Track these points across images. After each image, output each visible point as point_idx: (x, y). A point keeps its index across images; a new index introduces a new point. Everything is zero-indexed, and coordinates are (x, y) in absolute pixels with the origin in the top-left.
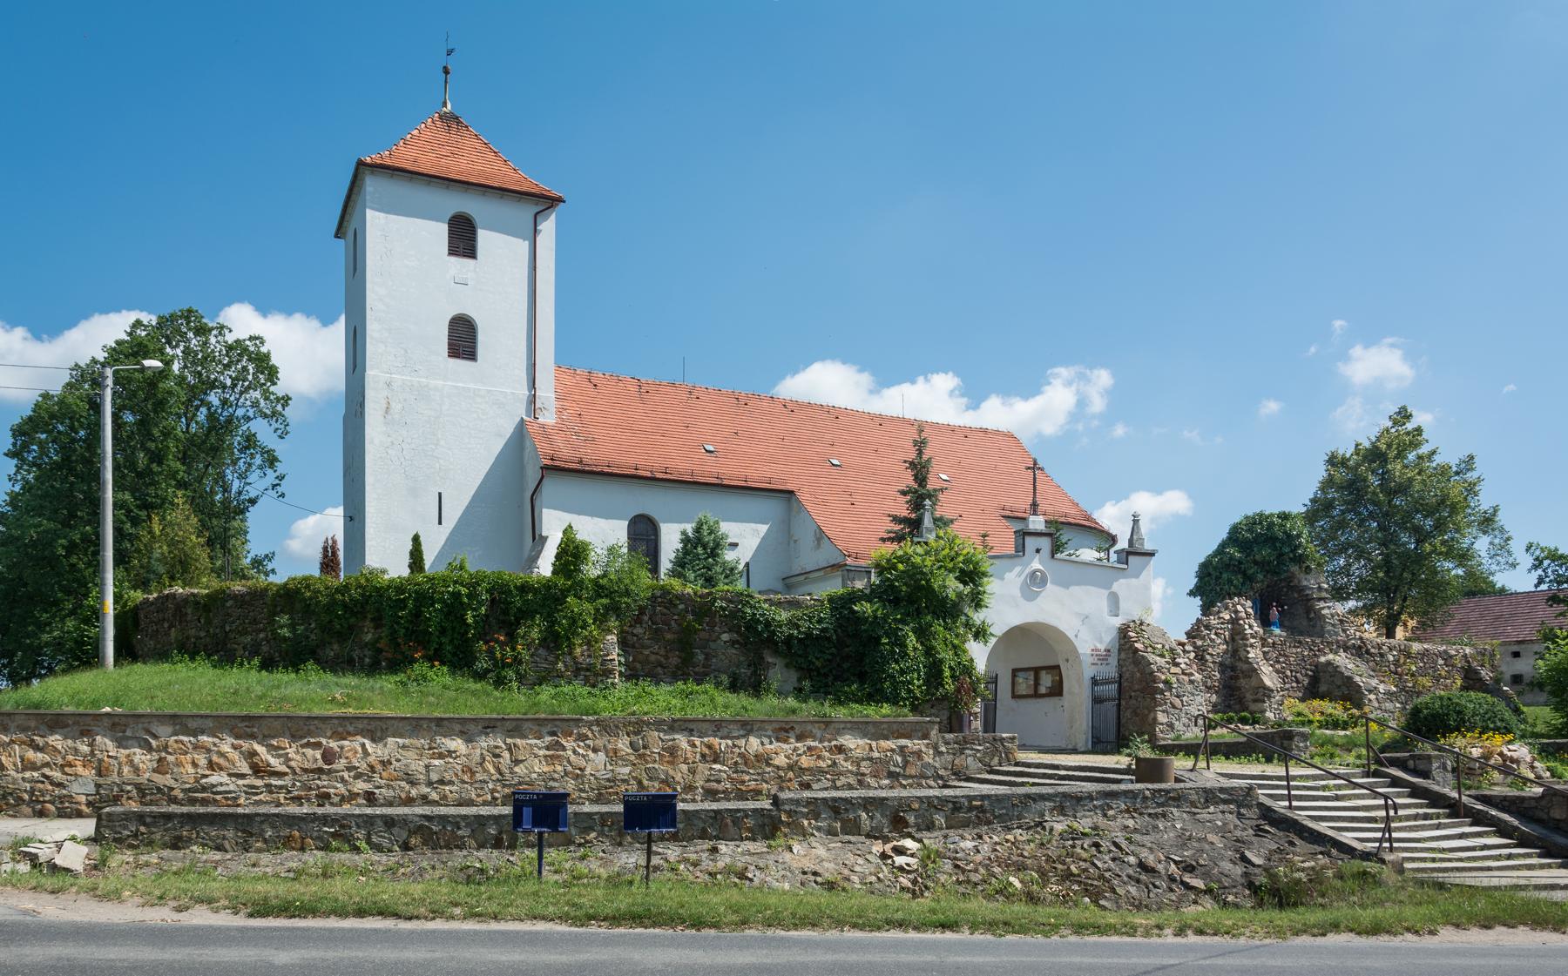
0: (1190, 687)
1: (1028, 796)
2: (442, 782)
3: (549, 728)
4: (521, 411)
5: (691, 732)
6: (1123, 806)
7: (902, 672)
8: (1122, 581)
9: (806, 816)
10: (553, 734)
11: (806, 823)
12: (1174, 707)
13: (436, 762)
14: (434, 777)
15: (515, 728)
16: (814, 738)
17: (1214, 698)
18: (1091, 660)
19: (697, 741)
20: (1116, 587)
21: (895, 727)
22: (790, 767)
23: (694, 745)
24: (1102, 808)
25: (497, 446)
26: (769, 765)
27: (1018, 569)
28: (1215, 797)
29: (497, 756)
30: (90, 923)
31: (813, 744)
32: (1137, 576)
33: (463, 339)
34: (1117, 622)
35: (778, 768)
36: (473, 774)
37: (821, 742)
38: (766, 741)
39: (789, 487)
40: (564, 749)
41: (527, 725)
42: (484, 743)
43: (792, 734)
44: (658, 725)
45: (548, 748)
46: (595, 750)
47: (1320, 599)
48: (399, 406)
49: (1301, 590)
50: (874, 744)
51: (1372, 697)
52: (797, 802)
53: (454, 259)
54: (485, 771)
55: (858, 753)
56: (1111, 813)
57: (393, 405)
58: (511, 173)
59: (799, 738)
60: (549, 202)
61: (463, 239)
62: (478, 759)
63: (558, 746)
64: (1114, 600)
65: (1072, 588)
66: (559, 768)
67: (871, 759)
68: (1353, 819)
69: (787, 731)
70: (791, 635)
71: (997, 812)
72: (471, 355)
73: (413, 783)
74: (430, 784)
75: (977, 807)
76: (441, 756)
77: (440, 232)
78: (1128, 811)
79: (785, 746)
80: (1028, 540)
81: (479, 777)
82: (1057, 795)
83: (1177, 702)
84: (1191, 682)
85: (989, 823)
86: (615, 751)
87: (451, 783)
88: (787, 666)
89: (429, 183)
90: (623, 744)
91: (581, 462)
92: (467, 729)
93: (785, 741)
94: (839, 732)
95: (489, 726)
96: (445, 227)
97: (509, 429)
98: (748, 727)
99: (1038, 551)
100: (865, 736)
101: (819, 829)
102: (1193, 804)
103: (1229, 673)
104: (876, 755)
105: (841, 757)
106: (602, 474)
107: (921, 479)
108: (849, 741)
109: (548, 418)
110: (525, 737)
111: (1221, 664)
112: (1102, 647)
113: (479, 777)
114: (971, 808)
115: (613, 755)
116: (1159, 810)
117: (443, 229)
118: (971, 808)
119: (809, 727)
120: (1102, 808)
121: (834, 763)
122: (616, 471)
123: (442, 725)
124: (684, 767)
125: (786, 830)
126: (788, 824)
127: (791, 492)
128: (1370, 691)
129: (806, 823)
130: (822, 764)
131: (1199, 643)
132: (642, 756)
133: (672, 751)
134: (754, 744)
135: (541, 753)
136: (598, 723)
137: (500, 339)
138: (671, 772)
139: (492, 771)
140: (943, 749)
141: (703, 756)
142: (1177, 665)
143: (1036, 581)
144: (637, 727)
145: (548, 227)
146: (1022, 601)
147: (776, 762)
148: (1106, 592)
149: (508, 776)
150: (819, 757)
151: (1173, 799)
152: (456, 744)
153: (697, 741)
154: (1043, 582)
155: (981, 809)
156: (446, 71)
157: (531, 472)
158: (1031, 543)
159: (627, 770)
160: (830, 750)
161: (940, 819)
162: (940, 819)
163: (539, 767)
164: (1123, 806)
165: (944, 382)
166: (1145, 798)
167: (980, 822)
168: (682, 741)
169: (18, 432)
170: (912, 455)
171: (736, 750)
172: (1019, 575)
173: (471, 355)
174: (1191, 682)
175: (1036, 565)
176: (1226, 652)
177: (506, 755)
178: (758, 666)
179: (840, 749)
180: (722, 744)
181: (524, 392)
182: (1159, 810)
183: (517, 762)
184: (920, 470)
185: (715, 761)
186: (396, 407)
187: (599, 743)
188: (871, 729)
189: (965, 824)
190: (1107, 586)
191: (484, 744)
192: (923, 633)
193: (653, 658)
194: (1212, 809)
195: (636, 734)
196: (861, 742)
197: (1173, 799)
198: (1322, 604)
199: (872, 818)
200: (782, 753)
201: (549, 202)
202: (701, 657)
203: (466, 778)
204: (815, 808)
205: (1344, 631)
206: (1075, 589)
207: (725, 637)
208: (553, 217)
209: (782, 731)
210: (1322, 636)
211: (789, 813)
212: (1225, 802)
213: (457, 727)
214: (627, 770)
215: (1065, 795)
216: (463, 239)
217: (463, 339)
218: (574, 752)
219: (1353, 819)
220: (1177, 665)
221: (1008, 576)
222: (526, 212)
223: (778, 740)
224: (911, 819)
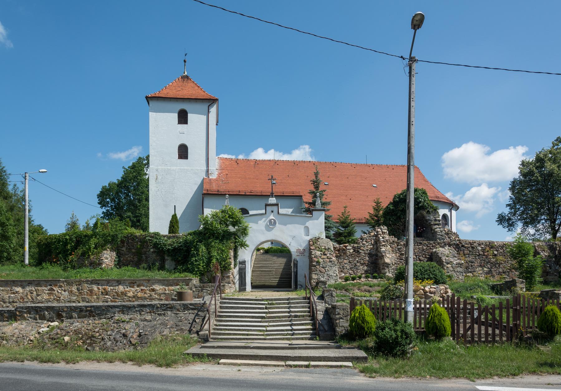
1: (109, 306)
2: (13, 302)
3: (49, 283)
4: (204, 175)
5: (98, 284)
6: (148, 311)
7: (196, 261)
8: (310, 221)
9: (25, 313)
10: (51, 285)
11: (26, 315)
12: (321, 272)
13: (12, 295)
14: (11, 300)
15: (38, 283)
16: (144, 286)
17: (366, 268)
19: (100, 287)
20: (307, 224)
21: (175, 281)
22: (134, 297)
23: (99, 289)
24: (139, 311)
25: (195, 188)
26: (126, 296)
27: (264, 219)
29: (32, 293)
31: (143, 288)
32: (317, 219)
33: (183, 152)
34: (308, 238)
35: (129, 297)
36: (23, 299)
38: (125, 287)
40: (54, 291)
41: (42, 282)
42: (28, 289)
43: (135, 285)
44: (87, 282)
45: (49, 290)
46: (65, 291)
47: (435, 224)
49: (427, 221)
50: (167, 288)
51: (449, 266)
52: (22, 308)
53: (180, 125)
54: (28, 298)
55: (160, 292)
56: (143, 313)
57: (159, 177)
58: (203, 93)
59: (138, 286)
60: (212, 101)
61: (183, 118)
62: (25, 294)
63: (52, 290)
64: (307, 229)
66: (52, 297)
67: (165, 294)
68: (253, 317)
69: (134, 283)
71: (97, 312)
72: (186, 157)
73: (5, 302)
74: (10, 303)
75: (89, 310)
76: (14, 293)
77: (175, 116)
78: (150, 312)
79: (132, 289)
80: (268, 208)
81: (25, 300)
82: (120, 306)
84: (330, 262)
85: (94, 316)
86: (71, 291)
87: (16, 302)
88: (172, 260)
89: (171, 101)
90: (74, 289)
91: (218, 191)
92: (23, 284)
93: (133, 287)
94: (153, 284)
95: (30, 283)
96: (177, 115)
97: (199, 182)
98: (119, 282)
99: (272, 212)
100: (163, 285)
101: (31, 318)
103: (374, 257)
105: (153, 293)
107: (317, 188)
108: (158, 287)
109: (214, 176)
110: (41, 287)
113: (25, 300)
114: (87, 311)
115: (71, 292)
116: (163, 312)
117: (176, 115)
118: (87, 311)
119: (142, 282)
120: (139, 311)
122: (211, 192)
123: (15, 283)
124: (95, 297)
125: (19, 318)
126: (20, 316)
127: (301, 196)
128: (448, 263)
129: (26, 315)
130: (146, 295)
131: (356, 245)
132: (80, 293)
133: (91, 291)
134: (121, 288)
135: (47, 292)
136: (66, 281)
137: (196, 152)
138: (90, 299)
139: (30, 298)
140: (194, 290)
141: (102, 293)
142: (325, 255)
143: (272, 223)
144: (80, 283)
145: (213, 110)
147: (129, 295)
148: (303, 227)
149: (35, 300)
150: (145, 293)
151: (170, 308)
152: (19, 289)
153: (100, 287)
155: (91, 311)
156: (185, 61)
157: (205, 194)
158: (269, 208)
159: (75, 298)
160: (150, 291)
161: (75, 315)
162: (75, 315)
163: (46, 297)
164: (148, 311)
165: (260, 150)
166: (158, 308)
167: (90, 316)
168: (95, 288)
169: (99, 196)
170: (314, 178)
171: (114, 291)
172: (265, 221)
173: (186, 157)
174: (330, 262)
175: (272, 217)
177: (35, 293)
178: (163, 261)
179: (153, 290)
180: (109, 288)
181: (205, 168)
182: (163, 312)
183: (38, 295)
184: (316, 184)
185: (106, 295)
186: (160, 177)
187: (66, 288)
188: (166, 282)
189: (85, 317)
190: (303, 224)
191: (28, 289)
192: (208, 246)
193: (129, 259)
194: (186, 312)
195: (79, 285)
196: (161, 287)
197: (170, 308)
198: (436, 227)
199: (49, 314)
200: (131, 291)
201: (212, 101)
203: (21, 301)
204: (29, 310)
205: (449, 238)
206: (289, 226)
207: (152, 250)
208: (215, 106)
209: (132, 284)
210: (436, 240)
211: (20, 312)
212: (192, 309)
213: (20, 283)
214: (75, 298)
215: (124, 306)
216: (183, 118)
217: (183, 152)
218: (58, 292)
219: (253, 317)
220: (325, 255)
221: (259, 222)
222: (205, 106)
223: (130, 287)
224: (64, 315)
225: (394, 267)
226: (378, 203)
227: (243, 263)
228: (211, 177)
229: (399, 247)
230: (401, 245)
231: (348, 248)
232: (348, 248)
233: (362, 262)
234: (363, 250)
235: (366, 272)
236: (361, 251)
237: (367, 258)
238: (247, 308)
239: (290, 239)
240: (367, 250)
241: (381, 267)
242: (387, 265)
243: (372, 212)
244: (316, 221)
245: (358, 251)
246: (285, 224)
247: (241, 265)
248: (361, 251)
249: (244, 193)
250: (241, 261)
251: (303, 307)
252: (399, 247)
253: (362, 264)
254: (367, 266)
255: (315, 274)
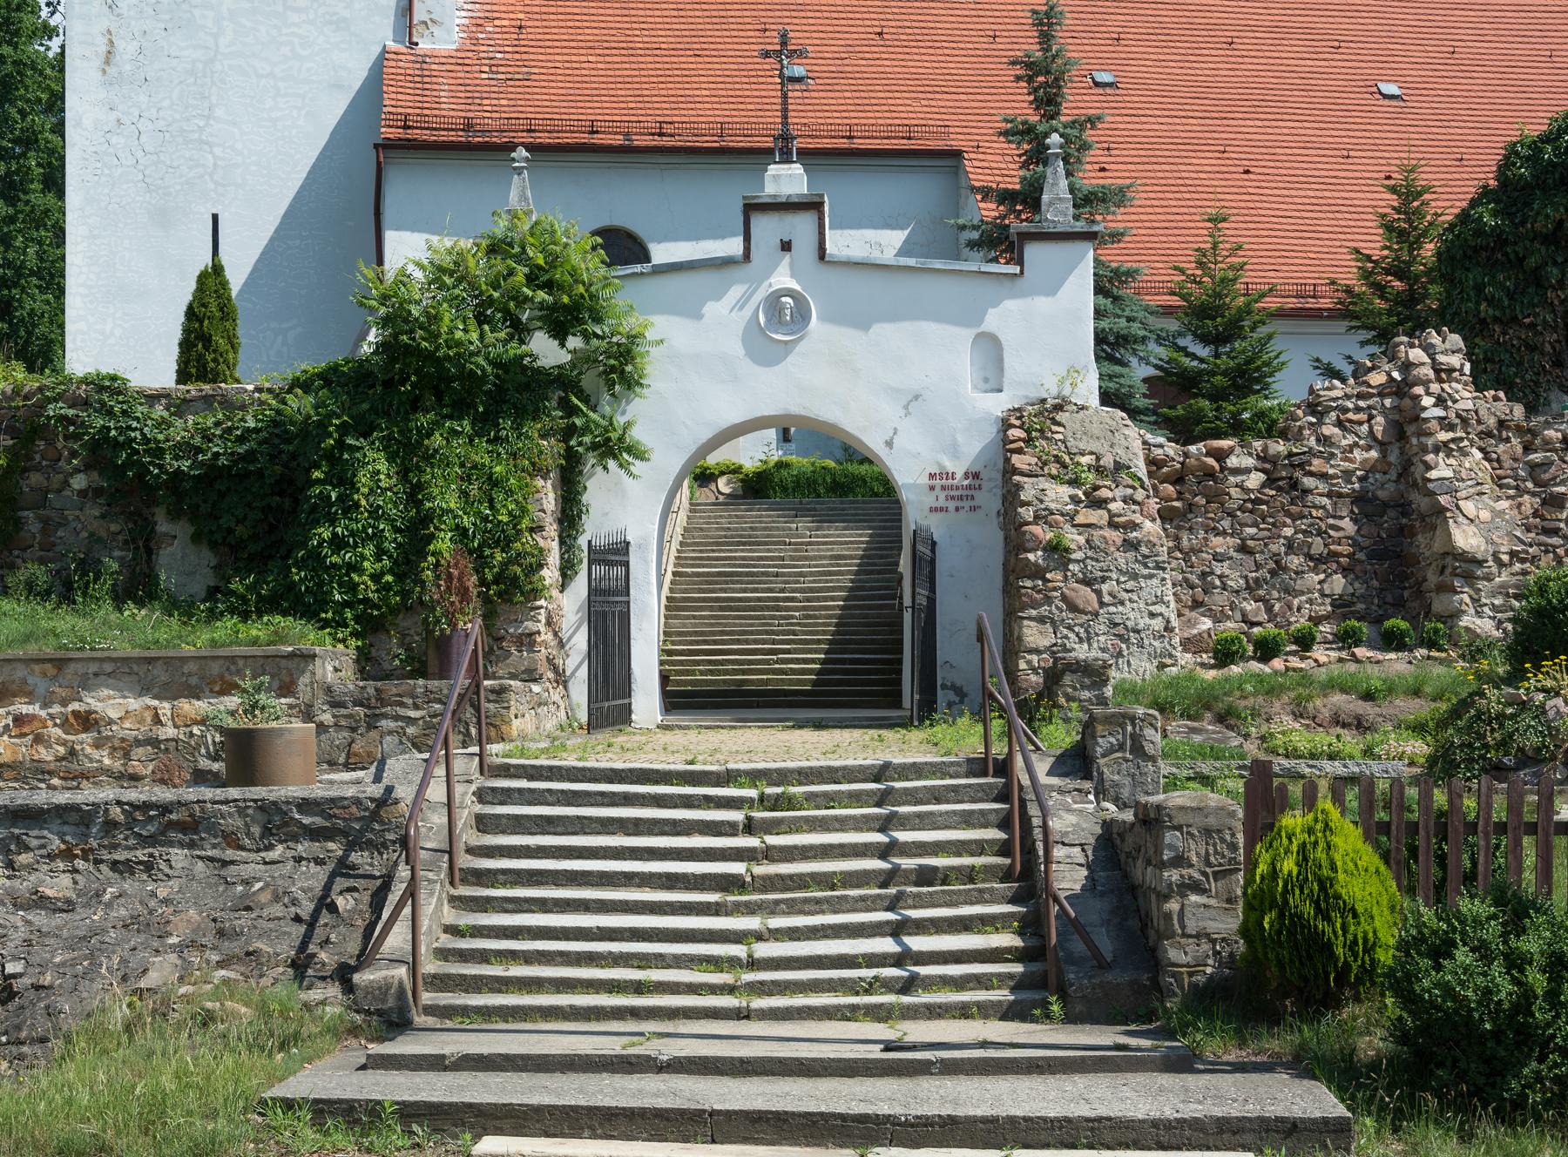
0: (1123, 559)
4: (383, 34)
6: (56, 844)
7: (338, 543)
8: (1010, 304)
12: (1073, 608)
16: (31, 697)
17: (1338, 583)
18: (930, 500)
20: (993, 320)
21: (215, 668)
25: (334, 108)
27: (736, 292)
28: (288, 822)
30: (1009, 1077)
31: (26, 709)
32: (1052, 291)
34: (998, 405)
37: (45, 706)
39: (955, 143)
48: (132, 48)
50: (165, 708)
55: (128, 730)
56: (24, 858)
57: (120, 44)
64: (991, 349)
65: (877, 328)
67: (154, 742)
70: (178, 471)
78: (68, 855)
83: (1085, 596)
94: (86, 683)
99: (786, 246)
100: (145, 689)
102: (231, 840)
103: (1389, 520)
104: (169, 732)
106: (626, 153)
107: (1048, 102)
108: (114, 705)
111: (1359, 499)
112: (958, 468)
116: (141, 855)
119: (20, 672)
121: (72, 753)
122: (425, 136)
127: (956, 154)
130: (44, 754)
131: (1279, 447)
140: (327, 718)
146: (747, 367)
150: (38, 739)
151: (181, 827)
154: (802, 314)
158: (767, 228)
160: (65, 725)
164: (56, 844)
166: (110, 826)
172: (741, 304)
175: (783, 278)
176: (1371, 469)
178: (144, 543)
179: (86, 721)
182: (141, 855)
186: (126, 48)
188: (161, 674)
190: (970, 317)
194: (278, 852)
196: (134, 704)
197: (181, 827)
202: (34, 526)
206: (885, 332)
207: (79, 482)
212: (315, 834)
220: (1100, 504)
225: (1504, 577)
226: (1409, 194)
227: (615, 554)
228: (424, 45)
229: (1536, 457)
230: (1547, 445)
231: (1233, 461)
232: (1233, 461)
233: (1318, 546)
234: (1323, 476)
235: (1342, 606)
236: (1309, 482)
237: (1348, 525)
238: (607, 826)
239: (889, 412)
240: (1347, 475)
241: (1432, 578)
242: (1467, 567)
243: (1375, 245)
244: (1042, 303)
245: (1294, 484)
246: (862, 322)
247: (598, 570)
248: (1309, 482)
249: (618, 140)
250: (599, 542)
251: (967, 820)
252: (1536, 457)
253: (1318, 561)
254: (1345, 571)
255: (1041, 620)
